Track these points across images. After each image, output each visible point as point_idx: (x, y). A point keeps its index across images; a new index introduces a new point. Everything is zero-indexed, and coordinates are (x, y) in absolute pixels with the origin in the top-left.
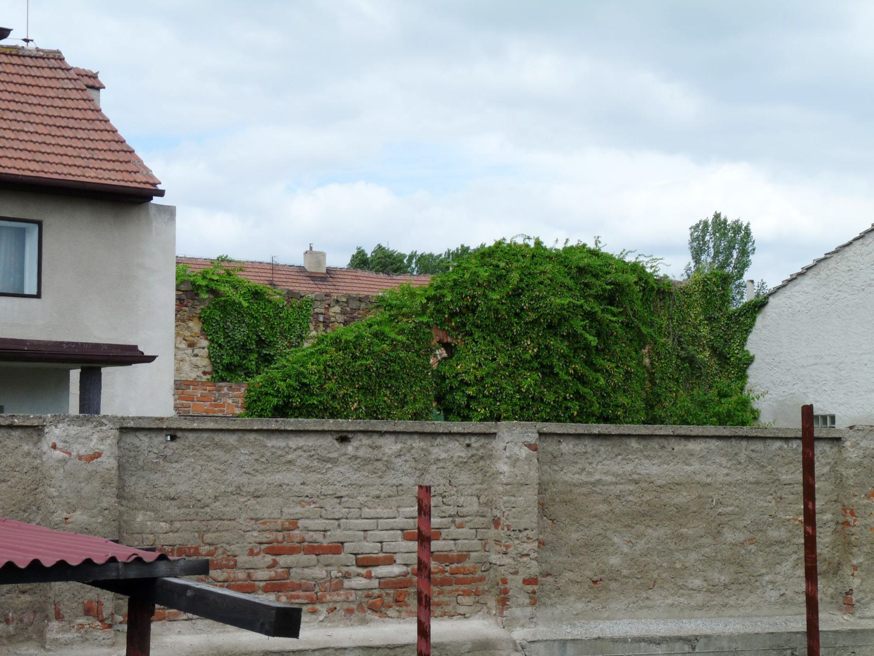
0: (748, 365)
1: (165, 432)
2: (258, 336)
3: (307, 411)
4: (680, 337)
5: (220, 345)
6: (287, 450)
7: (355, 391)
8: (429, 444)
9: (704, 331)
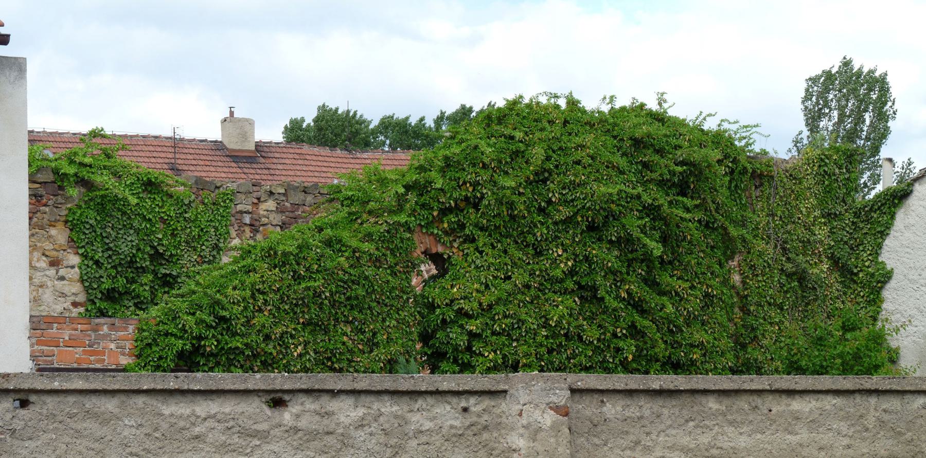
0: (885, 283)
1: (13, 396)
2: (153, 247)
3: (227, 359)
4: (785, 242)
5: (97, 263)
6: (193, 419)
7: (299, 327)
8: (406, 408)
9: (821, 233)
